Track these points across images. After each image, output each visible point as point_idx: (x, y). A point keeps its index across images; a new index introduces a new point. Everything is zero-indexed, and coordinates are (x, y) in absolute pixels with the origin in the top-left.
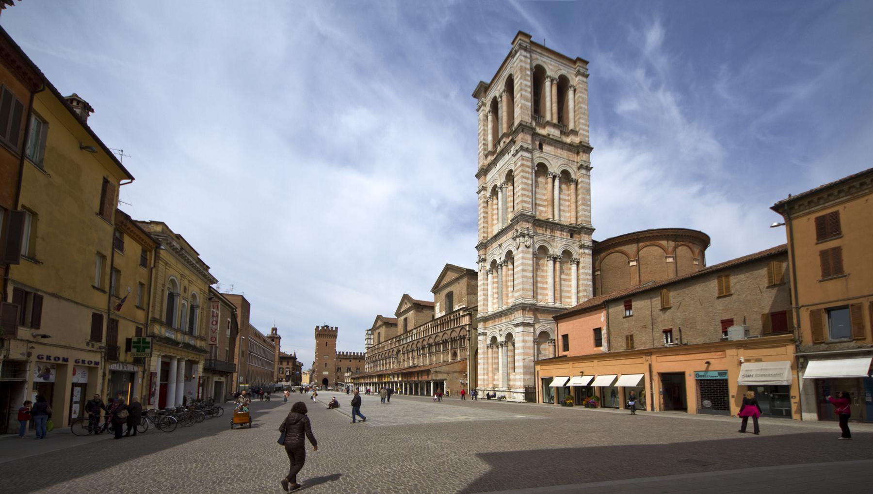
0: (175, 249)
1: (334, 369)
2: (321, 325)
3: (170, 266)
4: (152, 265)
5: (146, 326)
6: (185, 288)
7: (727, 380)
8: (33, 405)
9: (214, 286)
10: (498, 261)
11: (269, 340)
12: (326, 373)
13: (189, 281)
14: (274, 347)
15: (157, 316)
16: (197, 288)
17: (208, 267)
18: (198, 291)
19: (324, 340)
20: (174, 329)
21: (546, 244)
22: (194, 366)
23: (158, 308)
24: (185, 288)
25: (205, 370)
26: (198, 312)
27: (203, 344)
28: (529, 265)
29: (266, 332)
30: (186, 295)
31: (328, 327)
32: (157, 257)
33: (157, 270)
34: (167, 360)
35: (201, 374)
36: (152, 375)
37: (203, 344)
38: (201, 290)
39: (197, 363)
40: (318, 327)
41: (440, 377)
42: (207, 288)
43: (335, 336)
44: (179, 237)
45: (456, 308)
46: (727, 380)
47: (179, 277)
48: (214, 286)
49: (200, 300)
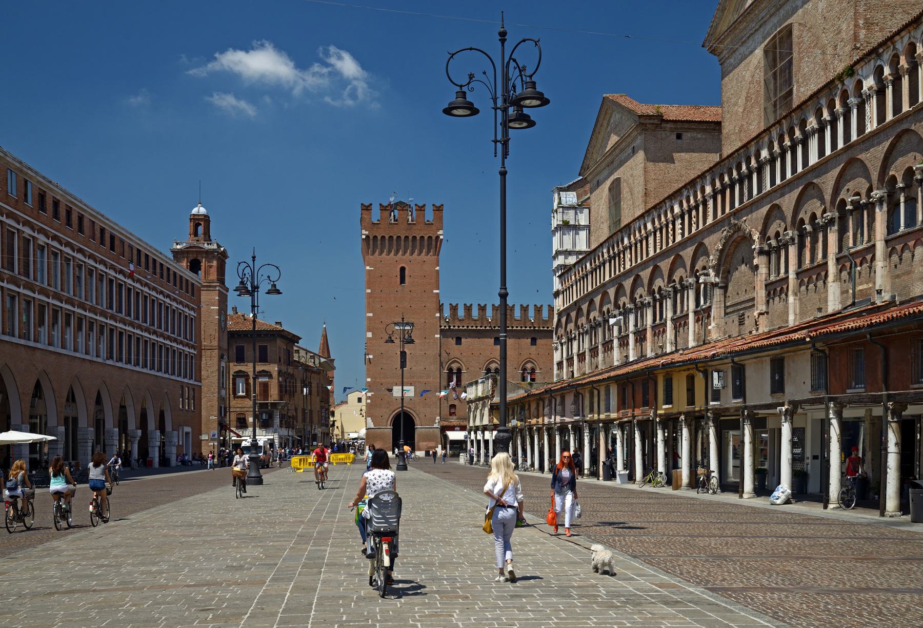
1: (434, 375)
11: (182, 268)
14: (193, 291)
19: (392, 261)
29: (167, 241)
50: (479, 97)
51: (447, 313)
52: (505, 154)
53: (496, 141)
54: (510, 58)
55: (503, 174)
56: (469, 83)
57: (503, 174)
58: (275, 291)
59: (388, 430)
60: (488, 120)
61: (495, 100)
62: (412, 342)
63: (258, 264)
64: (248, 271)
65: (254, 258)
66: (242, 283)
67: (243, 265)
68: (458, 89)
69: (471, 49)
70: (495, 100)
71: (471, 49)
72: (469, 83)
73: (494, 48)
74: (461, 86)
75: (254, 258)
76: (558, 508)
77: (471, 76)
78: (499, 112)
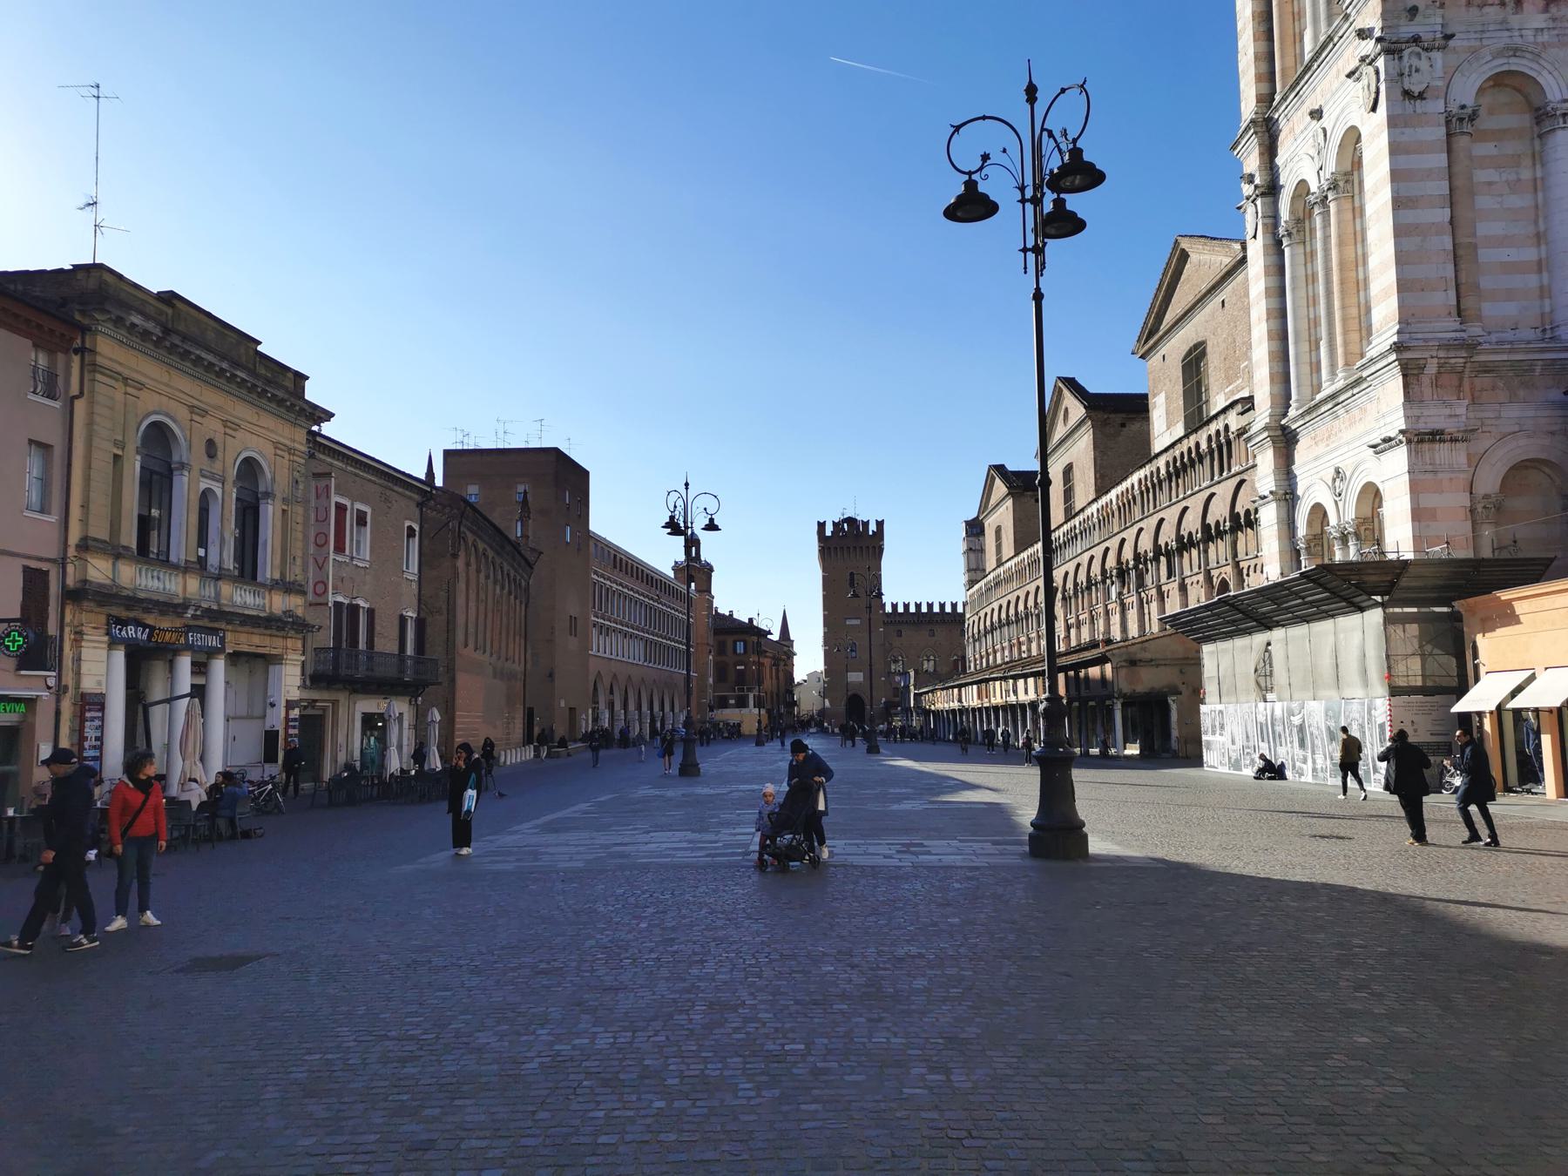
0: (145, 335)
2: (831, 517)
3: (141, 386)
4: (75, 390)
5: (62, 563)
6: (211, 443)
7: (448, 454)
8: (106, 786)
9: (327, 429)
10: (1314, 188)
12: (856, 677)
13: (225, 423)
15: (100, 531)
16: (260, 436)
17: (301, 378)
18: (269, 449)
20: (176, 567)
21: (1516, 64)
22: (158, 672)
23: (100, 501)
24: (211, 443)
25: (315, 679)
26: (270, 513)
27: (295, 603)
28: (1428, 174)
30: (217, 467)
31: (851, 521)
32: (91, 367)
33: (91, 403)
34: (202, 658)
35: (295, 694)
36: (93, 704)
37: (295, 603)
38: (276, 445)
39: (277, 660)
40: (821, 526)
41: (1148, 680)
42: (301, 435)
43: (878, 551)
44: (170, 298)
45: (1218, 402)
46: (448, 454)
47: (183, 413)
48: (327, 429)
49: (277, 474)
50: (997, 186)
51: (889, 609)
52: (1039, 272)
53: (1025, 250)
54: (1043, 129)
55: (1038, 297)
56: (981, 169)
57: (1038, 297)
58: (711, 526)
59: (842, 708)
60: (1011, 223)
61: (1022, 189)
62: (1093, 177)
63: (692, 492)
64: (680, 503)
65: (687, 485)
66: (672, 518)
67: (674, 496)
68: (966, 177)
69: (984, 118)
70: (1022, 189)
71: (984, 118)
72: (981, 169)
73: (1018, 113)
74: (970, 173)
75: (687, 485)
76: (52, 629)
77: (985, 157)
78: (1029, 207)
